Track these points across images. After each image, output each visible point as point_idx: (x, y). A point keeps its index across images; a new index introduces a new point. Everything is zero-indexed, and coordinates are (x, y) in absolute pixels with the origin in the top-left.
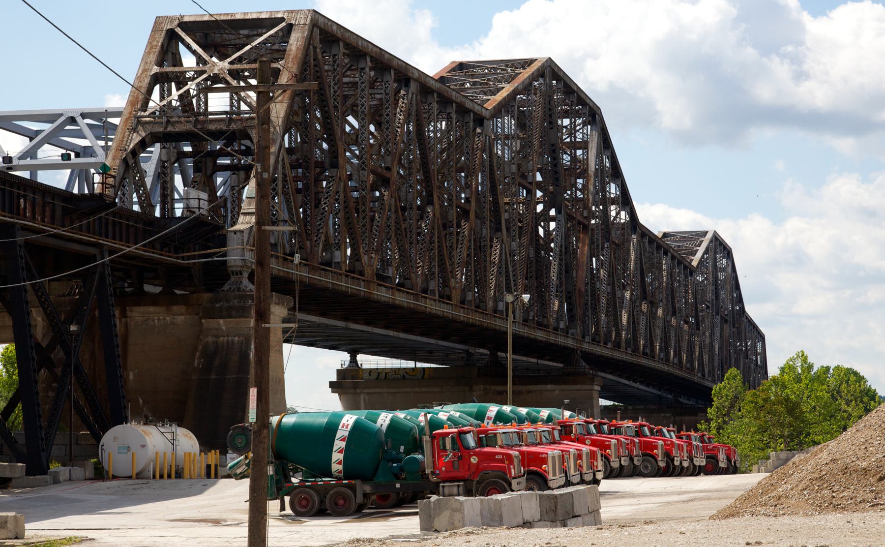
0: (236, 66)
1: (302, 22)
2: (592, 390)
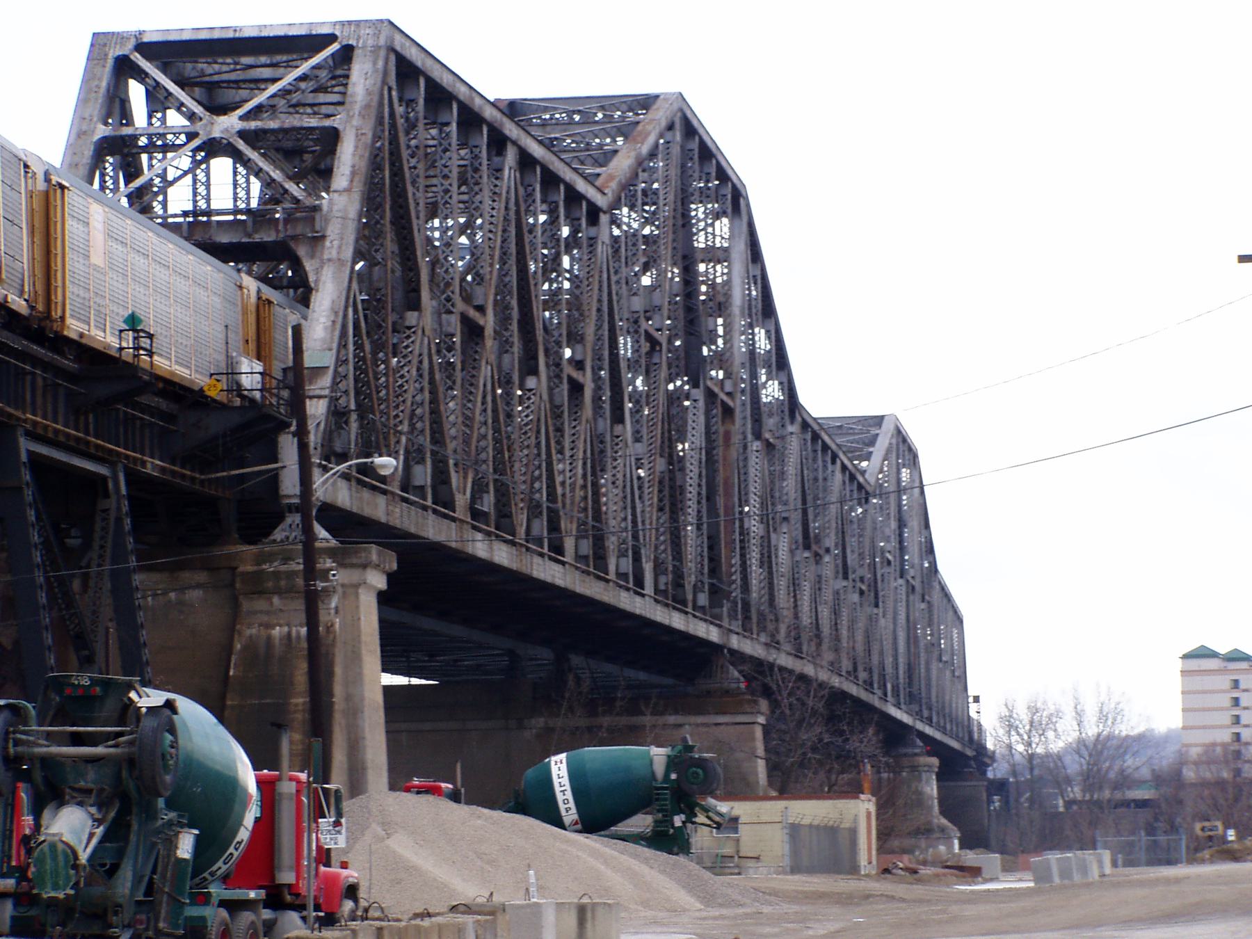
0: (253, 125)
1: (370, 42)
2: (754, 723)
